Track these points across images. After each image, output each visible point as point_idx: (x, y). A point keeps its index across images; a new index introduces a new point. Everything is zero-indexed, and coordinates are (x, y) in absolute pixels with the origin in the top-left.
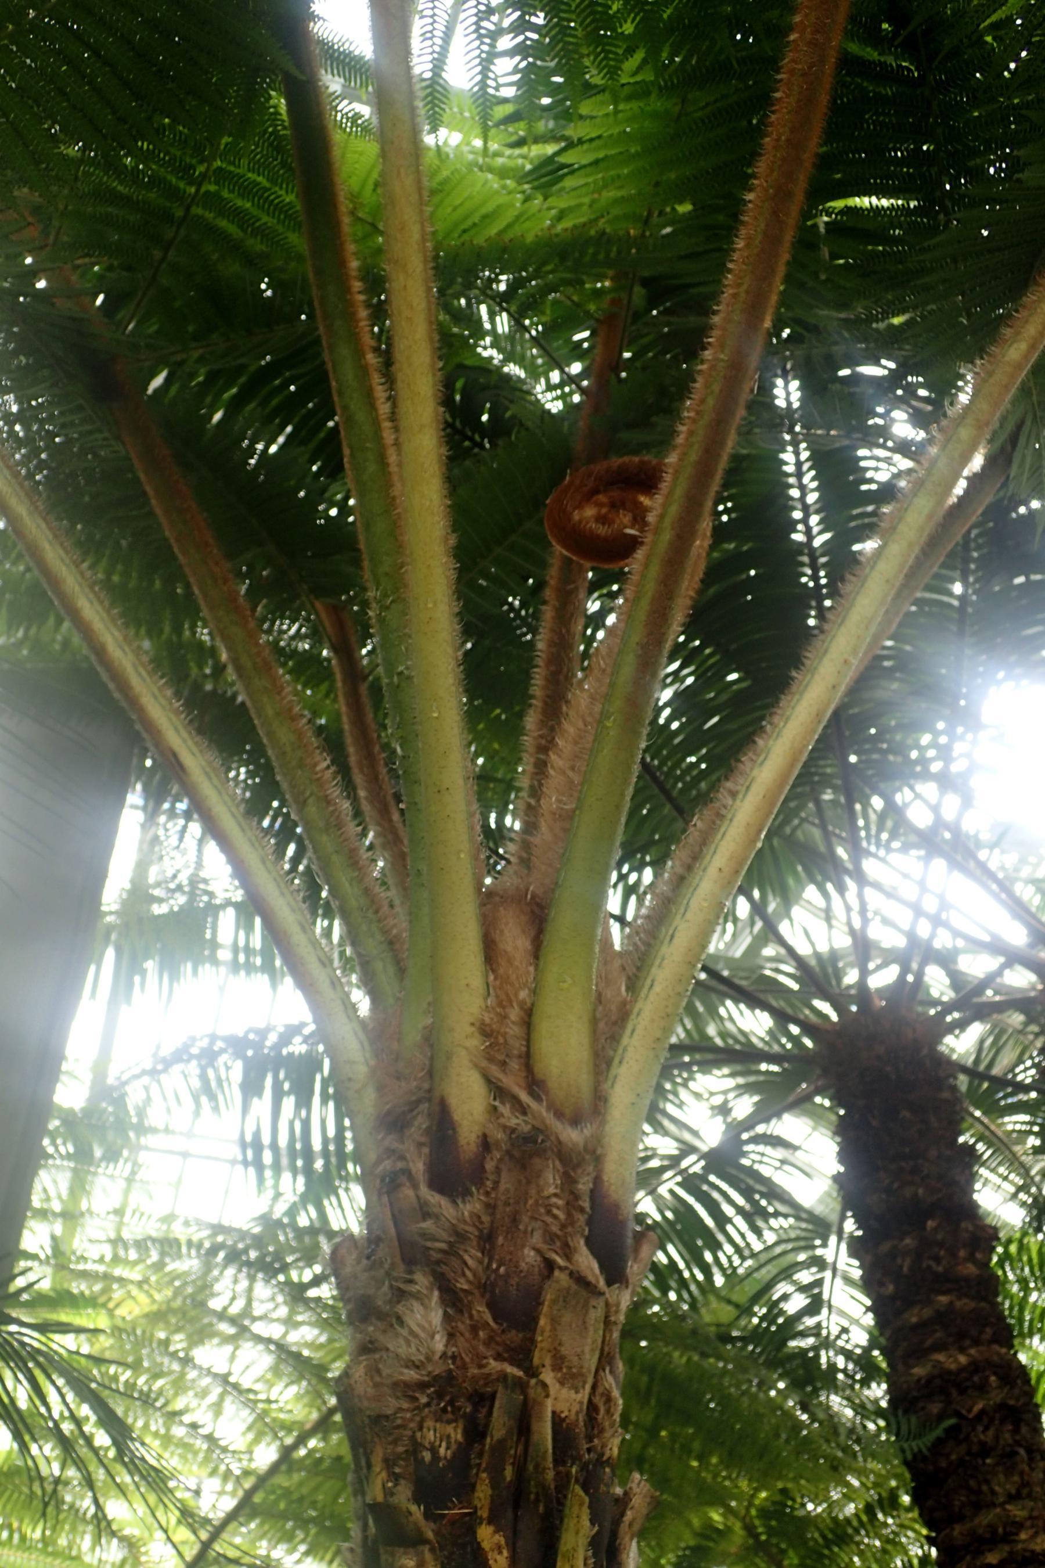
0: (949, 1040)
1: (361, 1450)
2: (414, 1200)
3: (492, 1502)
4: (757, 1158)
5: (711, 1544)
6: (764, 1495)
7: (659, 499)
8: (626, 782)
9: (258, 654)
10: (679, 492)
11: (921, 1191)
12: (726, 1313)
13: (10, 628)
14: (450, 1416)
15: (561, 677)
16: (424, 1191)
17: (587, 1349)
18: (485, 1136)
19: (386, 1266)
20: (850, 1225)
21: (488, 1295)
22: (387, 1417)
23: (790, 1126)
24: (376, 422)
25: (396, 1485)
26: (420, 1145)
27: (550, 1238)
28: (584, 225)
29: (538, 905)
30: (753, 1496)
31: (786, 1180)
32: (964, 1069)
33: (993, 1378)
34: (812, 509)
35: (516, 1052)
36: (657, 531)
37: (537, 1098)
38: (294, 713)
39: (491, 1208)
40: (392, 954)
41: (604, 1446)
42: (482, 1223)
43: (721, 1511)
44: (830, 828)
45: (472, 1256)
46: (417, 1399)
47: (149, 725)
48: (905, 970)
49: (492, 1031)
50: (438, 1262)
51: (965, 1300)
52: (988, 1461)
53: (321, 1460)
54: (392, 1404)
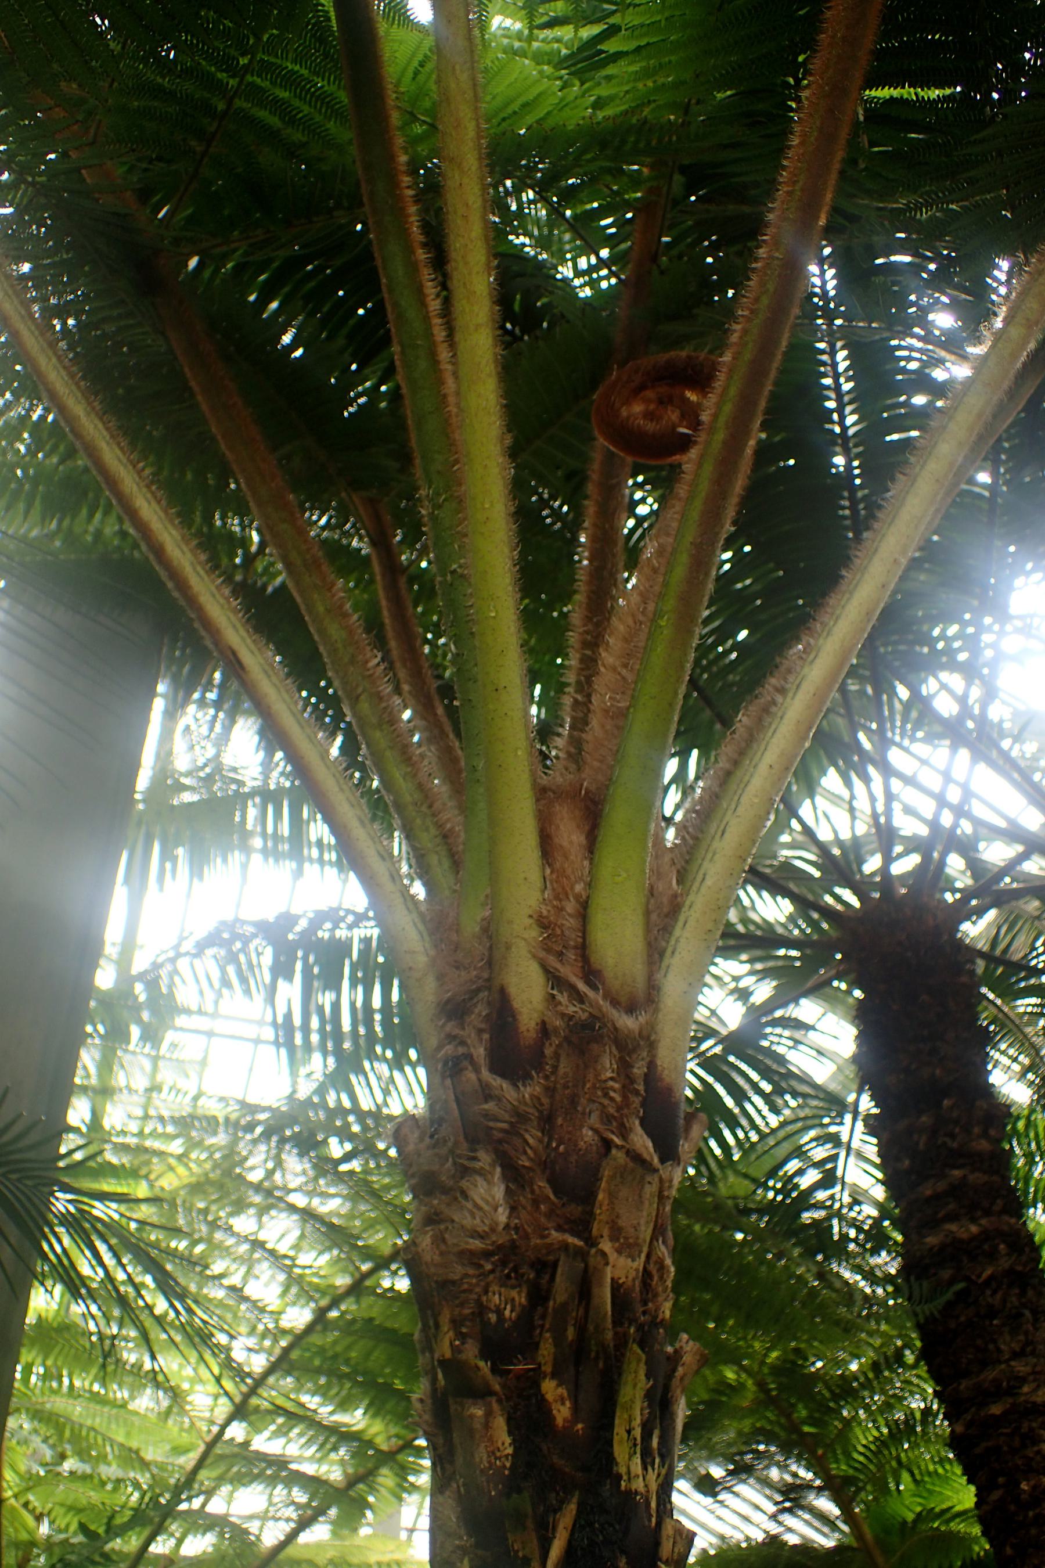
0: (966, 927)
1: (429, 1312)
2: (477, 1083)
3: (555, 1359)
4: (775, 1039)
5: (724, 1399)
6: (774, 1354)
7: (713, 398)
8: (679, 680)
9: (308, 550)
10: (733, 391)
11: (938, 1072)
12: (743, 1187)
13: (43, 519)
14: (513, 1281)
15: (606, 573)
16: (486, 1074)
17: (643, 1221)
18: (544, 1023)
19: (450, 1144)
20: (867, 1104)
21: (548, 1172)
22: (453, 1282)
23: (807, 1009)
24: (426, 319)
25: (463, 1343)
26: (480, 1031)
27: (607, 1118)
28: (625, 113)
29: (593, 801)
30: (766, 1355)
31: (800, 1060)
32: (981, 954)
33: (1002, 1246)
34: (846, 399)
35: (572, 943)
36: (712, 430)
37: (594, 987)
38: (337, 610)
39: (550, 1091)
40: (452, 851)
41: (657, 1309)
42: (542, 1105)
43: (735, 1368)
44: (856, 718)
45: (532, 1137)
46: (481, 1266)
47: (207, 623)
48: (927, 858)
49: (550, 923)
50: (500, 1141)
51: (977, 1174)
52: (995, 1322)
53: (354, 1321)
54: (457, 1271)
